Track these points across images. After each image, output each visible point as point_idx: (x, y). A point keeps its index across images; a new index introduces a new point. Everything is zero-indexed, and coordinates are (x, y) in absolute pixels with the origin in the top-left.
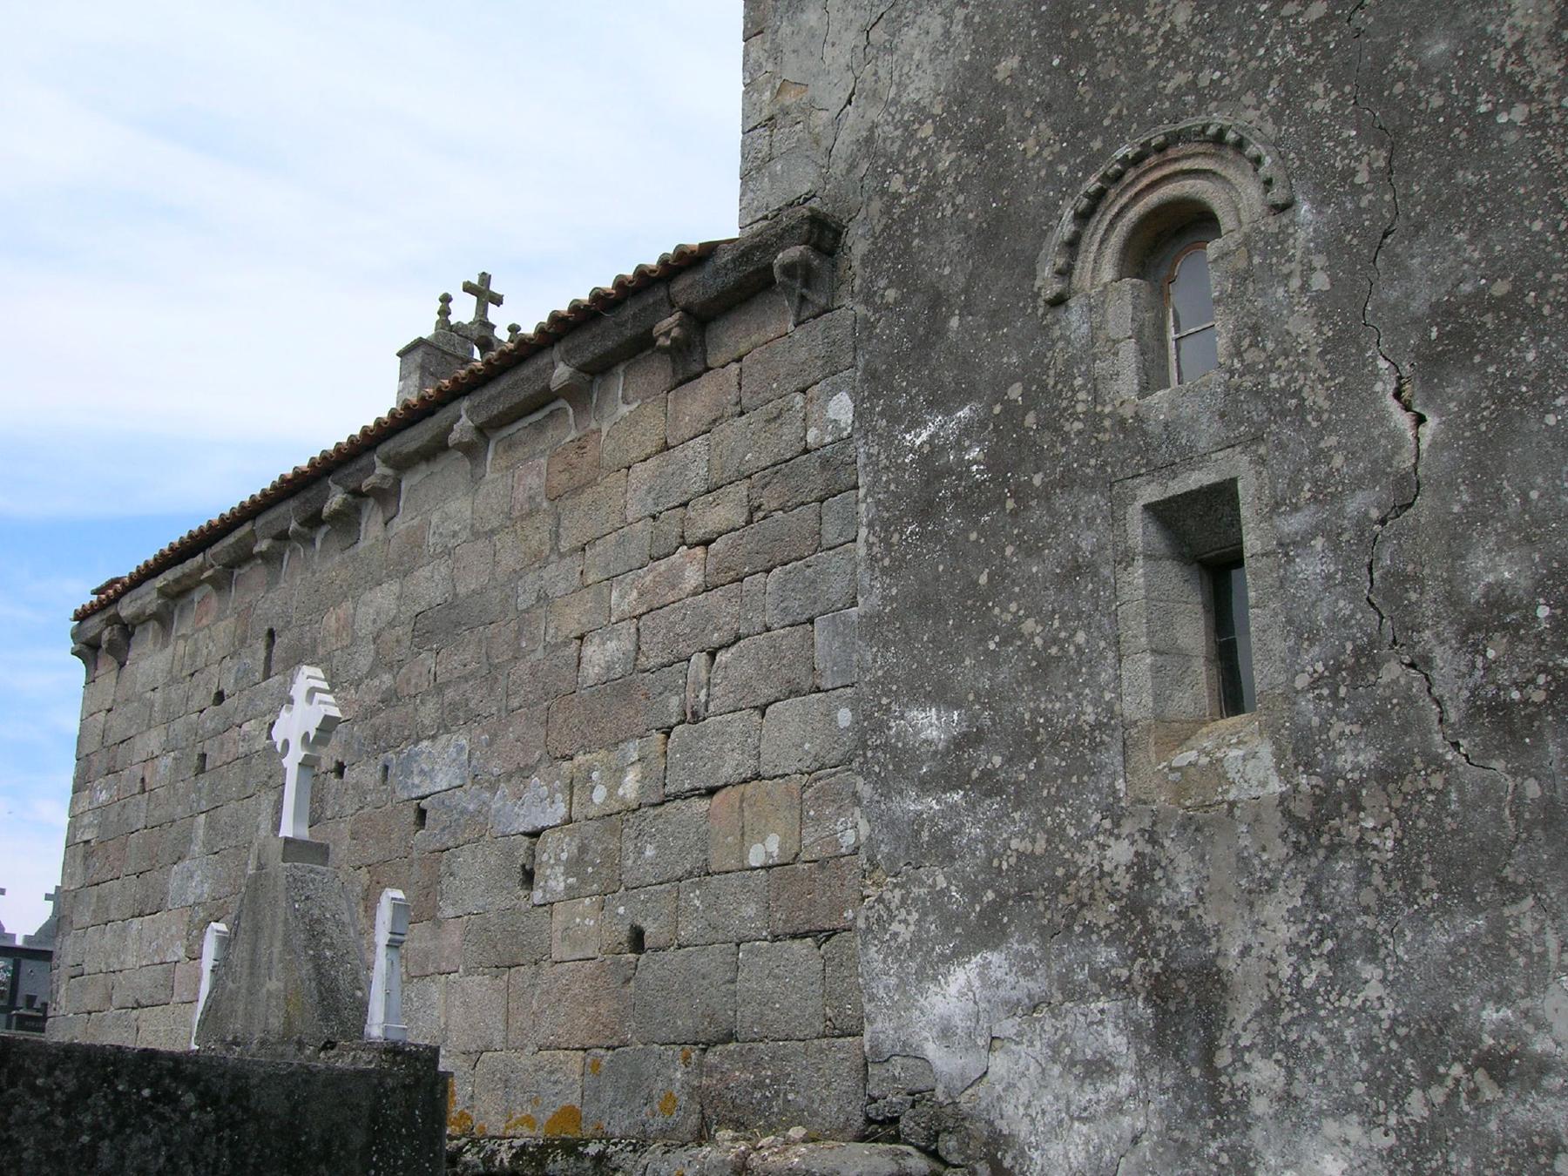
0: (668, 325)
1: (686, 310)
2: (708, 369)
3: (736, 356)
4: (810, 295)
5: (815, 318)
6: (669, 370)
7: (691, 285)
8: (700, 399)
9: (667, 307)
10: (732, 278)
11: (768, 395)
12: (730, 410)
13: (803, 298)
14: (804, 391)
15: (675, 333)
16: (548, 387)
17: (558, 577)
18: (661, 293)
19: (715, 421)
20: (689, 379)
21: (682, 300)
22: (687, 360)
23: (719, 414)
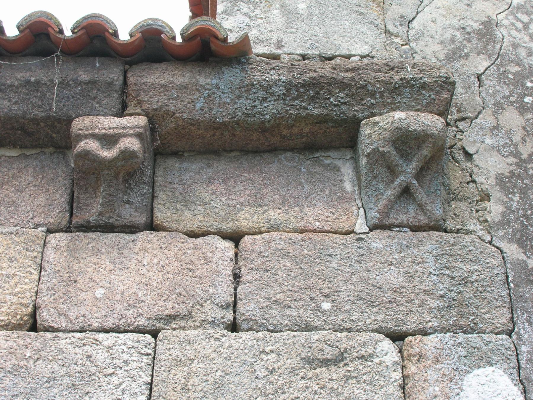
0: (110, 131)
1: (154, 120)
2: (152, 226)
3: (228, 226)
4: (421, 195)
5: (415, 229)
6: (61, 199)
7: (184, 87)
8: (128, 272)
9: (114, 101)
10: (272, 108)
11: (307, 315)
12: (211, 312)
13: (406, 192)
14: (397, 337)
15: (132, 144)
16: (69, 121)
17: (258, 315)
18: (113, 74)
19: (171, 318)
20: (108, 228)
21: (157, 101)
22: (108, 201)
23: (182, 309)
